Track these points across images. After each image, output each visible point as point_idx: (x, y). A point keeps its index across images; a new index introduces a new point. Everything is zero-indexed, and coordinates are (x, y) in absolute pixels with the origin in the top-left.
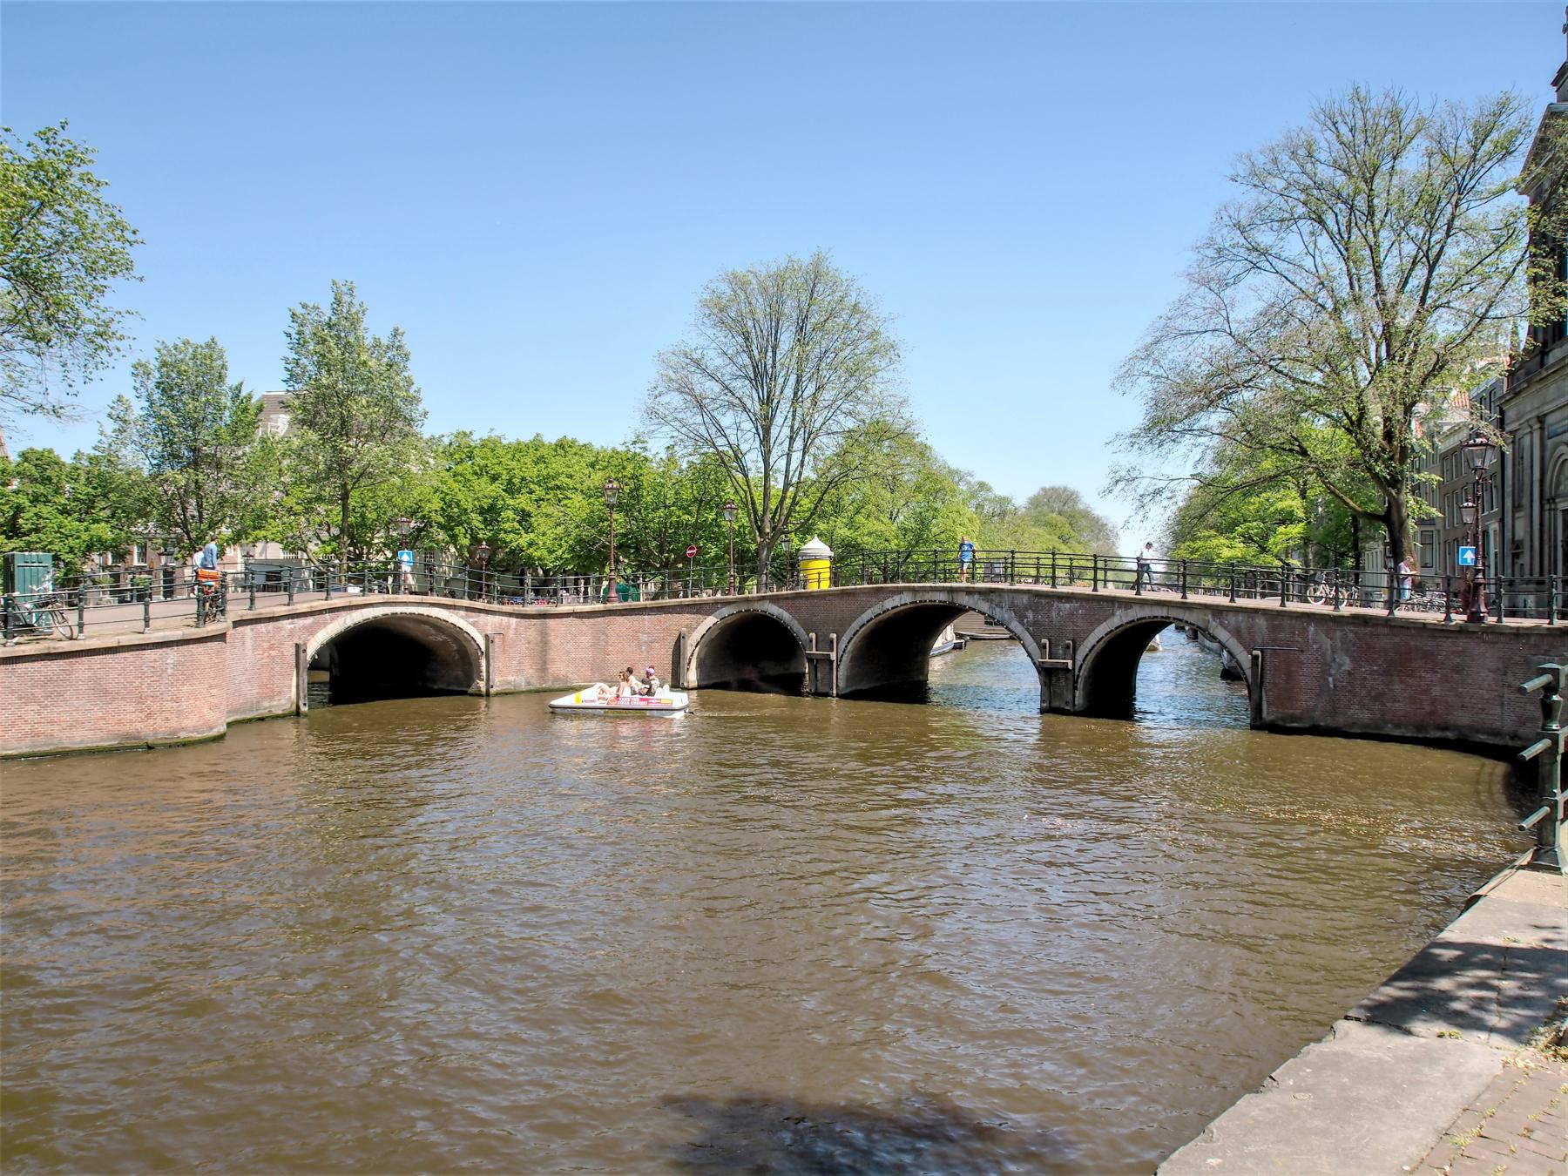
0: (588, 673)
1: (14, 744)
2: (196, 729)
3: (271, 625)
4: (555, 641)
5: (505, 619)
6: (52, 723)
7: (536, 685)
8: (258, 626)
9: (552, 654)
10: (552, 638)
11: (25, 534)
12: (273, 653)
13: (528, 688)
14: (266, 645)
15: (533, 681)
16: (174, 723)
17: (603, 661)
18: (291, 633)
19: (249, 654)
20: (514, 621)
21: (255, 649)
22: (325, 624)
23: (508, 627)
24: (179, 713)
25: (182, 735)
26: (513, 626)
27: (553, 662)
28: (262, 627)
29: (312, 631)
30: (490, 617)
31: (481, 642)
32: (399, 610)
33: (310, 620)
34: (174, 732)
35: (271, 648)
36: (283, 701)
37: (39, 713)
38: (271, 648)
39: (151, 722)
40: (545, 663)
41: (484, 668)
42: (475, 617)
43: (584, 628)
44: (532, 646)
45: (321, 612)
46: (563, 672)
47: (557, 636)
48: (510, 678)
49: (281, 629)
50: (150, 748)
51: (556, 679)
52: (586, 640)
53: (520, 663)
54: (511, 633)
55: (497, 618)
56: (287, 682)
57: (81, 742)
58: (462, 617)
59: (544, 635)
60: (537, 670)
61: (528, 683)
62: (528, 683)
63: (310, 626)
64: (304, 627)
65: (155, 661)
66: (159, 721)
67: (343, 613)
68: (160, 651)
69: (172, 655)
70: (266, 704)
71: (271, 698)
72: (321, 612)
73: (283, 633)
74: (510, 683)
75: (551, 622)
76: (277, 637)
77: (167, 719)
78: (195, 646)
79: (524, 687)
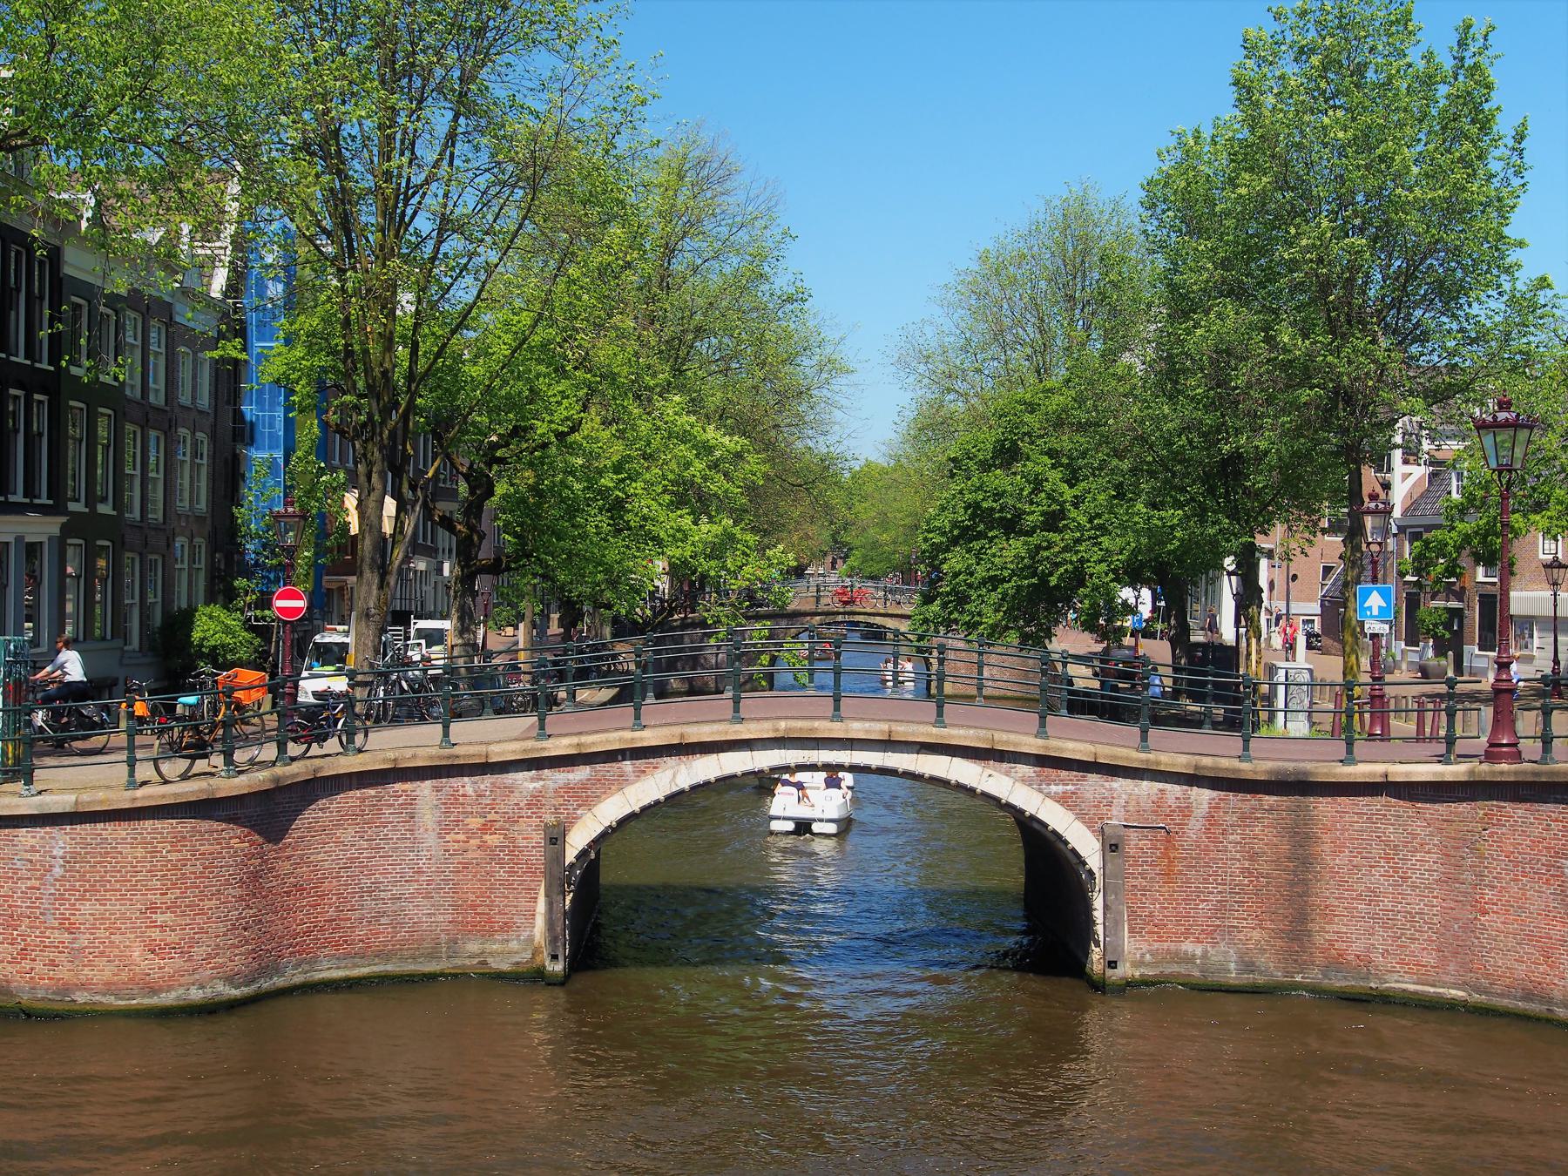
0: (1430, 959)
2: (109, 988)
3: (485, 782)
4: (1333, 858)
5: (1173, 790)
7: (1271, 969)
8: (455, 782)
9: (1326, 892)
11: (1030, 533)
12: (493, 840)
13: (1247, 979)
14: (475, 823)
15: (1262, 960)
16: (64, 973)
17: (1469, 927)
18: (535, 801)
21: (444, 830)
22: (622, 782)
23: (1186, 810)
24: (76, 954)
25: (81, 998)
27: (1328, 914)
28: (467, 785)
29: (585, 797)
30: (1120, 785)
33: (581, 773)
34: (66, 989)
35: (486, 828)
36: (514, 945)
38: (486, 828)
39: (26, 964)
41: (1098, 915)
42: (1064, 783)
43: (1419, 828)
44: (1265, 868)
46: (1357, 947)
47: (1338, 849)
48: (1188, 947)
49: (511, 789)
50: (29, 1016)
51: (1336, 963)
52: (1425, 865)
53: (1221, 908)
54: (1195, 827)
55: (1147, 788)
56: (523, 904)
58: (1025, 781)
59: (1301, 843)
61: (1248, 966)
62: (1248, 966)
63: (583, 786)
64: (568, 788)
65: (33, 850)
66: (39, 966)
67: (671, 761)
68: (41, 832)
69: (60, 840)
70: (473, 947)
71: (488, 934)
73: (514, 799)
74: (1189, 959)
75: (1324, 807)
76: (502, 808)
77: (53, 964)
78: (110, 826)
79: (1233, 976)
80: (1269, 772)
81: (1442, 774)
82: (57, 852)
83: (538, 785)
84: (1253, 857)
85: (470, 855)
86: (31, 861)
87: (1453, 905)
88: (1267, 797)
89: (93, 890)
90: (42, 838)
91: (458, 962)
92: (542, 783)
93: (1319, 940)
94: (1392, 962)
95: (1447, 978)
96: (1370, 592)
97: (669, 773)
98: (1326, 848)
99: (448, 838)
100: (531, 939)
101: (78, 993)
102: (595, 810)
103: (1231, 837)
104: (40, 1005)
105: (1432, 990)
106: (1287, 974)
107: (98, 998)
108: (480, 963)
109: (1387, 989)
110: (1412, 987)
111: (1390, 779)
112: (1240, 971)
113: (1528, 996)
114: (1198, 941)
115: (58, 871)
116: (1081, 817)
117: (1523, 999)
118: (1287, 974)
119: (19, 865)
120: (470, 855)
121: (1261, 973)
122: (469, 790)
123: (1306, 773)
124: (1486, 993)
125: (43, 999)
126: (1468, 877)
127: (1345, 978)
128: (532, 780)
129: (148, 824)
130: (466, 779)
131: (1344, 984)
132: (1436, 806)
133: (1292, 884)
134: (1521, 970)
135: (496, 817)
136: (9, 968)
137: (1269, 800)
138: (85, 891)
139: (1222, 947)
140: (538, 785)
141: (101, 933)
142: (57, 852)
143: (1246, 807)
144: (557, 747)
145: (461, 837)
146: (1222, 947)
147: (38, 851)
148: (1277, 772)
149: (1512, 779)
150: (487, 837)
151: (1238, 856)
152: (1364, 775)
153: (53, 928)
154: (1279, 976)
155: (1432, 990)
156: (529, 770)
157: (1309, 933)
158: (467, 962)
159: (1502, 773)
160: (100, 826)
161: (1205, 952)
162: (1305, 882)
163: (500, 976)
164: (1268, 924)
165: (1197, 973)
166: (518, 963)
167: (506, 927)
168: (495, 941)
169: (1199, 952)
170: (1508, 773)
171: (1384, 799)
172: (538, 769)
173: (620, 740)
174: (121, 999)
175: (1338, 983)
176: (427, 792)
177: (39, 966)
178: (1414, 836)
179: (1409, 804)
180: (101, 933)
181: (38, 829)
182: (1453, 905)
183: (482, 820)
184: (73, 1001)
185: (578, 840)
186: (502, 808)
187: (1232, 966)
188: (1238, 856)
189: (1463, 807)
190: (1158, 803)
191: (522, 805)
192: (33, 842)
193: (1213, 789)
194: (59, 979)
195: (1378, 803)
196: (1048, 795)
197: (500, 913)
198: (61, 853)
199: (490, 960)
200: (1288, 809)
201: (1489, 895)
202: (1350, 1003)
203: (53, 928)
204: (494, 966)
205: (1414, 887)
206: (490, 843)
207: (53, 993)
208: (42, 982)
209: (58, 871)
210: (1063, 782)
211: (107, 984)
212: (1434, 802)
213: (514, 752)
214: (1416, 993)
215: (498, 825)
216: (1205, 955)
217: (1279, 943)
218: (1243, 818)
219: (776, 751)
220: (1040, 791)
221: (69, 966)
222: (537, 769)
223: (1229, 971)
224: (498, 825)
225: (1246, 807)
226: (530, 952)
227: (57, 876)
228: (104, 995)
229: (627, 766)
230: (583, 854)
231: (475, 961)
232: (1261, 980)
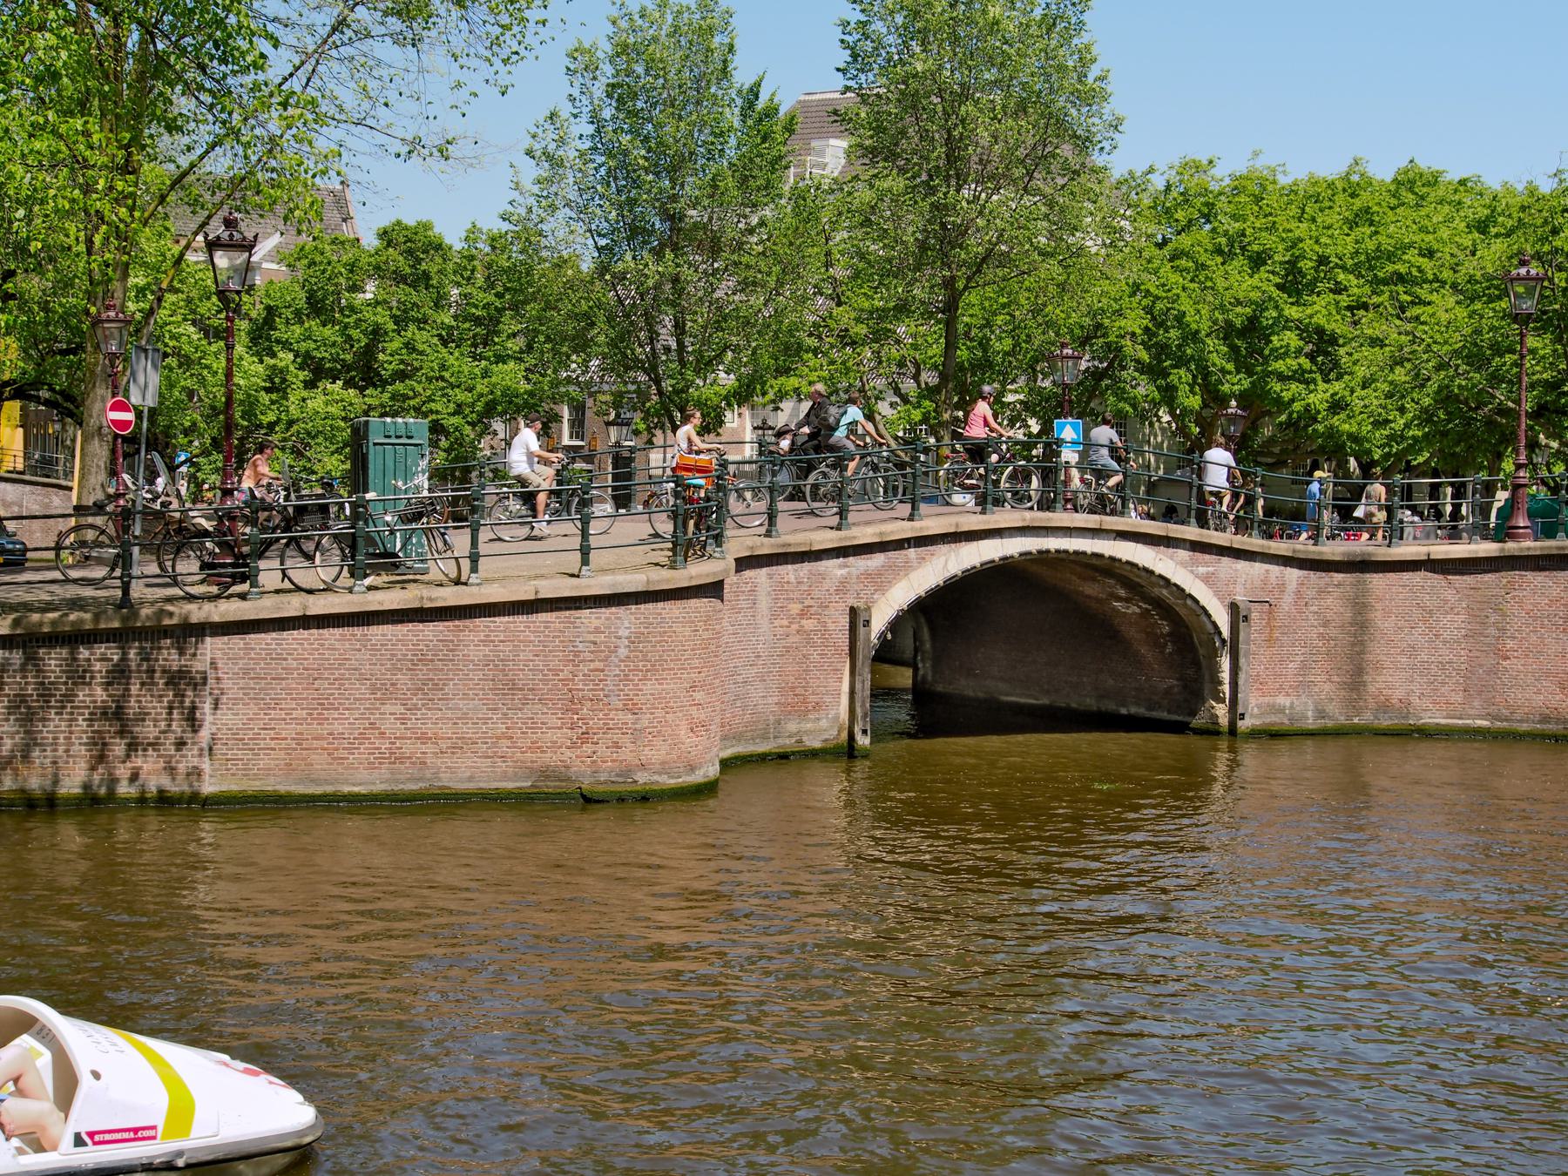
0: (1458, 698)
1: (363, 774)
2: (664, 769)
3: (805, 568)
4: (1383, 622)
5: (1275, 570)
6: (424, 739)
7: (1338, 715)
9: (1377, 651)
10: (1377, 616)
12: (809, 624)
13: (1320, 723)
14: (795, 608)
16: (627, 755)
18: (842, 587)
19: (764, 624)
20: (1293, 574)
21: (774, 616)
22: (907, 568)
23: (1282, 587)
24: (637, 734)
25: (642, 778)
26: (1292, 586)
27: (1379, 668)
28: (789, 572)
29: (880, 582)
30: (1242, 565)
31: (1222, 619)
32: (1053, 543)
33: (878, 560)
34: (627, 772)
35: (803, 614)
36: (824, 723)
37: (403, 720)
38: (803, 614)
40: (1359, 671)
43: (1450, 595)
44: (1333, 632)
45: (900, 544)
48: (1283, 701)
49: (823, 576)
51: (1385, 707)
52: (1454, 624)
53: (1304, 668)
54: (1287, 601)
55: (1258, 568)
57: (471, 779)
58: (1183, 564)
60: (1343, 685)
61: (1321, 713)
62: (1321, 713)
65: (597, 631)
66: (602, 749)
68: (605, 612)
70: (792, 727)
71: (803, 715)
72: (900, 544)
73: (827, 584)
74: (1281, 710)
76: (816, 593)
77: (617, 745)
79: (1311, 723)
80: (1344, 554)
81: (1477, 552)
82: (623, 633)
83: (843, 572)
84: (1326, 624)
85: (792, 639)
86: (595, 643)
87: (1478, 654)
88: (1336, 575)
89: (653, 670)
90: (607, 619)
91: (780, 741)
92: (847, 570)
93: (1371, 689)
94: (1426, 703)
95: (1472, 712)
96: (1064, 426)
97: (943, 559)
98: (1378, 614)
99: (777, 623)
100: (837, 717)
101: (639, 774)
102: (888, 595)
103: (1312, 608)
104: (601, 788)
105: (1460, 722)
106: (1349, 718)
107: (656, 778)
108: (797, 742)
109: (1423, 724)
110: (1443, 721)
111: (1432, 557)
112: (1316, 718)
113: (1545, 719)
114: (1288, 695)
115: (623, 652)
116: (1217, 594)
117: (1540, 722)
118: (1349, 718)
119: (581, 647)
120: (792, 639)
121: (1330, 718)
122: (792, 578)
123: (1369, 554)
124: (1507, 720)
125: (605, 782)
126: (1492, 631)
127: (1391, 718)
128: (840, 567)
129: (694, 603)
130: (790, 566)
131: (1390, 723)
132: (1465, 577)
133: (1353, 645)
134: (1539, 700)
135: (811, 602)
136: (568, 753)
137: (1338, 577)
138: (647, 671)
139: (1303, 698)
140: (843, 572)
141: (659, 713)
142: (623, 633)
143: (1322, 583)
144: (865, 536)
145: (785, 622)
146: (1303, 698)
147: (603, 632)
148: (1349, 554)
149: (1538, 553)
150: (804, 622)
151: (1316, 623)
152: (1412, 554)
153: (617, 710)
154: (1342, 720)
155: (1460, 722)
156: (838, 557)
157: (1364, 684)
158: (787, 742)
159: (1529, 549)
160: (660, 605)
161: (1292, 703)
162: (1362, 643)
163: (813, 754)
164: (1336, 679)
165: (1287, 722)
166: (826, 740)
167: (817, 706)
168: (808, 721)
169: (1288, 704)
170: (1535, 549)
171: (1422, 573)
172: (845, 556)
173: (912, 529)
174: (673, 777)
175: (1385, 722)
176: (764, 579)
177: (602, 749)
178: (1446, 602)
179: (1441, 577)
180: (659, 713)
181: (603, 610)
182: (1478, 654)
183: (800, 606)
184: (636, 782)
185: (879, 621)
186: (816, 593)
187: (1310, 714)
188: (1316, 623)
189: (1488, 577)
190: (1265, 581)
191: (832, 591)
192: (596, 623)
193: (1301, 568)
194: (621, 762)
195: (1418, 577)
196: (1197, 576)
197: (813, 694)
198: (627, 633)
199: (804, 739)
200: (1351, 584)
201: (1510, 644)
202: (1395, 739)
203: (617, 710)
204: (808, 743)
205: (1445, 642)
206: (806, 627)
207: (617, 775)
208: (604, 765)
209: (623, 652)
210: (1206, 564)
211: (663, 763)
212: (1462, 574)
213: (831, 540)
214: (1447, 725)
215: (812, 610)
216: (1292, 707)
217: (1343, 693)
218: (1320, 592)
219: (1019, 539)
220: (1192, 572)
221: (631, 747)
222: (844, 557)
223: (1307, 718)
224: (812, 610)
225: (1322, 583)
226: (836, 729)
227: (622, 657)
228: (660, 774)
229: (912, 553)
230: (882, 635)
231: (793, 740)
232: (1330, 724)
